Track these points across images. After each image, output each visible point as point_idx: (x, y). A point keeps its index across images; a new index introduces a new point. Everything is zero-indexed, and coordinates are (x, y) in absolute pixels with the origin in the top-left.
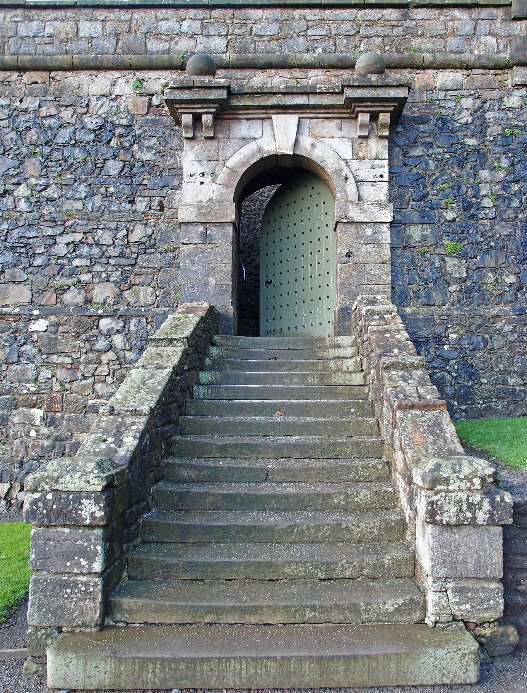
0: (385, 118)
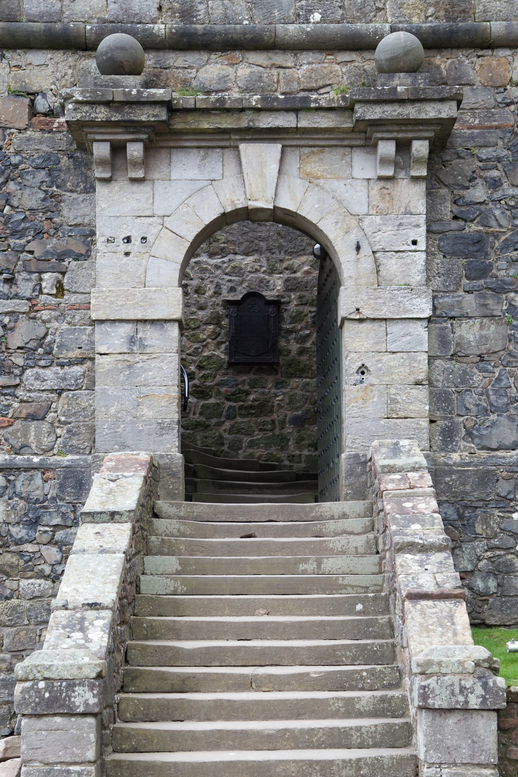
0: (420, 148)
